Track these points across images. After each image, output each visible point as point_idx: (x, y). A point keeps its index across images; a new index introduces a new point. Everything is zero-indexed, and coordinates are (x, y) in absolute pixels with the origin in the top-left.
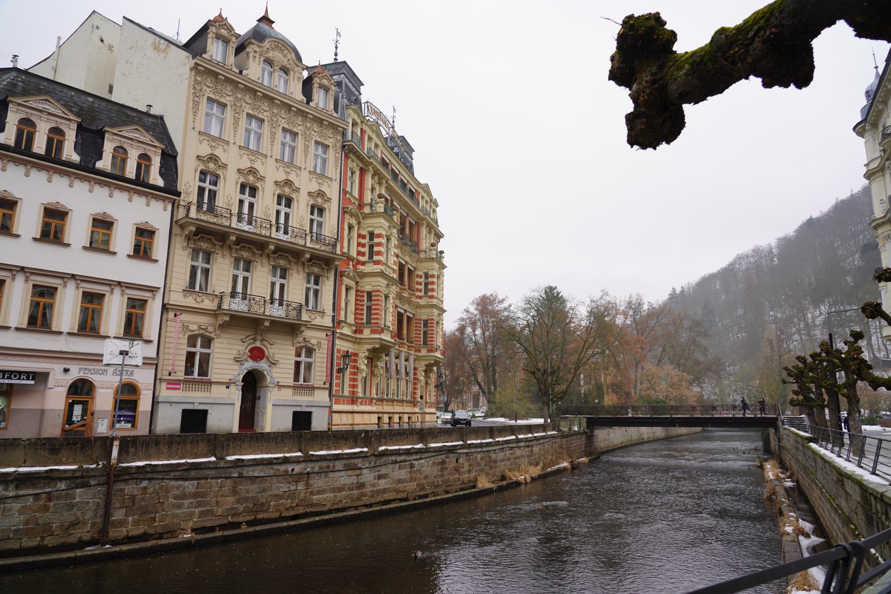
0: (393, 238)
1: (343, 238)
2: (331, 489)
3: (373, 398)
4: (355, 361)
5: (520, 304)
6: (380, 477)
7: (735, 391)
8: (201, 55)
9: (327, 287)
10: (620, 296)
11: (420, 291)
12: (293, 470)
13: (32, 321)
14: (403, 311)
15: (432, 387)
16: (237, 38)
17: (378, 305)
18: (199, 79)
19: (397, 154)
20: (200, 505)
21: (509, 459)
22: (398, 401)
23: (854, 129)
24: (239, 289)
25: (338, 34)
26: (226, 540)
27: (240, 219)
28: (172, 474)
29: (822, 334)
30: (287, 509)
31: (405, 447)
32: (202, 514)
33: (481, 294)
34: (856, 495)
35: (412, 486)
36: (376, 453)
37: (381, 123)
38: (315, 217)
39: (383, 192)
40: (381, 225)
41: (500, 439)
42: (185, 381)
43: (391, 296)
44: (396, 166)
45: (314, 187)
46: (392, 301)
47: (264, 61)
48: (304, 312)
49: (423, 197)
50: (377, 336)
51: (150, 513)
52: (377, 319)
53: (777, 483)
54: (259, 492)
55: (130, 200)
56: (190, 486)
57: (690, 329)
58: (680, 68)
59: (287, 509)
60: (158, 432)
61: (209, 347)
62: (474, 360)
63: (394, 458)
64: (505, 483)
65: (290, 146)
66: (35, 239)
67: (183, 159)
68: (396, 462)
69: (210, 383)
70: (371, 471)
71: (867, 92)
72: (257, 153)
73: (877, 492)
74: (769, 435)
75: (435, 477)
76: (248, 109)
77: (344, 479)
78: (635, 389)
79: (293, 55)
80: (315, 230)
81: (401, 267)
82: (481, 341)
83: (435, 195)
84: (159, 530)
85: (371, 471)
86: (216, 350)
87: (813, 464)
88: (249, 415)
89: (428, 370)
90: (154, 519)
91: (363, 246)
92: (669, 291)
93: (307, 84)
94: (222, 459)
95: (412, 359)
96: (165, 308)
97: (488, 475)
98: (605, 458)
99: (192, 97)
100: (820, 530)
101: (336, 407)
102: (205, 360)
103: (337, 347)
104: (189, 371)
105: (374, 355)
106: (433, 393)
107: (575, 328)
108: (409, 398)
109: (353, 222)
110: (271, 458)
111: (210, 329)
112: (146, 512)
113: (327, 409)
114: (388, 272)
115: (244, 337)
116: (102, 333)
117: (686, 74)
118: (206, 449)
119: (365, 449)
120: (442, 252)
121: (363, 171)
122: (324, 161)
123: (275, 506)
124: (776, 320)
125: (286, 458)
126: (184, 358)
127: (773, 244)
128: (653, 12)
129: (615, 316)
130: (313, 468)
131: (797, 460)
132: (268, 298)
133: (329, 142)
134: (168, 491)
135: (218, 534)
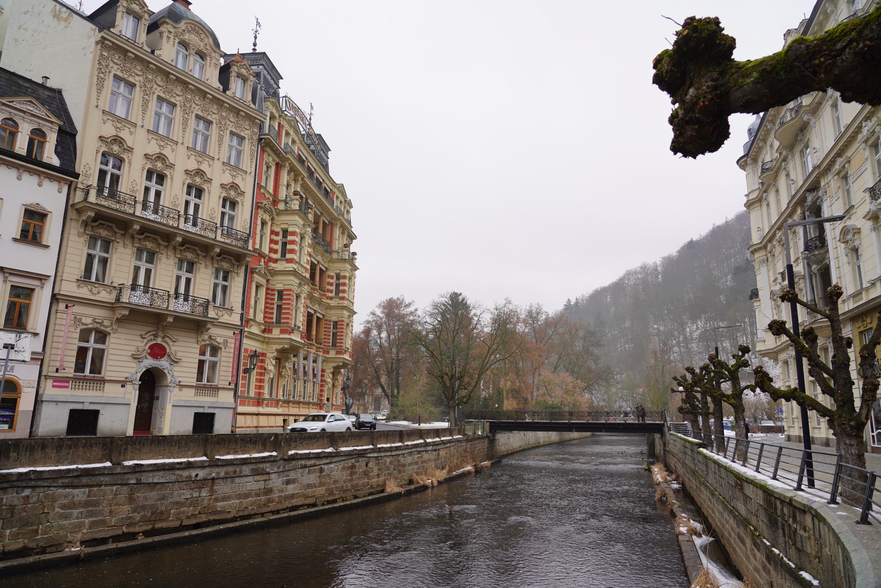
0: (307, 237)
1: (255, 233)
2: (237, 495)
3: (280, 400)
4: (263, 361)
5: (428, 309)
6: (288, 482)
7: (621, 398)
8: (109, 29)
9: (237, 284)
10: (522, 304)
11: (331, 291)
12: (197, 475)
14: (313, 312)
15: (338, 390)
16: (150, 15)
17: (289, 304)
18: (106, 54)
19: (313, 152)
20: (91, 514)
21: (417, 463)
22: (304, 403)
23: (737, 162)
24: (141, 281)
25: (258, 24)
26: (120, 552)
27: (145, 207)
28: (60, 482)
29: (698, 347)
30: (188, 517)
31: (315, 451)
32: (93, 524)
33: (388, 298)
34: (758, 498)
35: (321, 491)
36: (286, 457)
37: (299, 119)
38: (227, 210)
39: (299, 190)
40: (295, 223)
41: (409, 443)
42: (75, 379)
43: (303, 296)
44: (313, 164)
45: (227, 179)
46: (303, 301)
47: (179, 43)
48: (211, 308)
49: (337, 197)
50: (287, 336)
51: (32, 524)
52: (288, 318)
53: (666, 485)
54: (159, 500)
56: (80, 494)
57: (584, 339)
58: (748, 76)
59: (188, 517)
60: (40, 434)
61: (104, 343)
62: (378, 363)
63: (303, 462)
64: (412, 487)
65: (203, 134)
67: (83, 139)
68: (305, 466)
69: (103, 381)
70: (279, 476)
71: (749, 130)
72: (166, 139)
73: (785, 497)
74: (654, 439)
75: (345, 482)
76: (159, 92)
77: (251, 484)
78: (532, 394)
79: (211, 40)
80: (226, 223)
81: (313, 266)
82: (386, 345)
83: (350, 196)
84: (41, 544)
85: (279, 476)
86: (112, 346)
87: (703, 468)
88: (145, 415)
89: (336, 372)
90: (36, 532)
91: (276, 243)
92: (564, 302)
93: (224, 73)
94: (118, 464)
95: (320, 360)
96: (55, 298)
97: (396, 478)
98: (505, 461)
99: (96, 72)
100: (709, 529)
101: (241, 409)
102: (99, 356)
103: (244, 347)
104: (80, 366)
105: (282, 357)
106: (340, 396)
107: (478, 334)
108: (315, 401)
109: (267, 217)
110: (174, 463)
111: (106, 323)
112: (27, 524)
113: (232, 411)
114: (301, 271)
115: (143, 333)
117: (753, 82)
118: (100, 454)
119: (274, 454)
120: (354, 254)
121: (278, 167)
122: (239, 153)
123: (175, 514)
124: (659, 333)
125: (189, 463)
126: (75, 353)
127: (658, 263)
128: (712, 16)
129: (515, 325)
130: (218, 473)
131: (684, 464)
132: (172, 292)
133: (245, 133)
134: (54, 500)
135: (111, 546)
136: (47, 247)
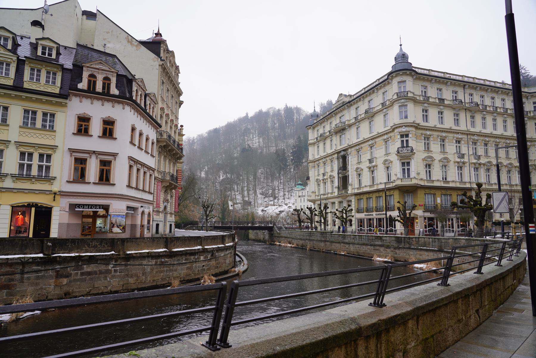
13: (101, 179)
55: (92, 103)
116: (111, 182)
136: (91, 136)
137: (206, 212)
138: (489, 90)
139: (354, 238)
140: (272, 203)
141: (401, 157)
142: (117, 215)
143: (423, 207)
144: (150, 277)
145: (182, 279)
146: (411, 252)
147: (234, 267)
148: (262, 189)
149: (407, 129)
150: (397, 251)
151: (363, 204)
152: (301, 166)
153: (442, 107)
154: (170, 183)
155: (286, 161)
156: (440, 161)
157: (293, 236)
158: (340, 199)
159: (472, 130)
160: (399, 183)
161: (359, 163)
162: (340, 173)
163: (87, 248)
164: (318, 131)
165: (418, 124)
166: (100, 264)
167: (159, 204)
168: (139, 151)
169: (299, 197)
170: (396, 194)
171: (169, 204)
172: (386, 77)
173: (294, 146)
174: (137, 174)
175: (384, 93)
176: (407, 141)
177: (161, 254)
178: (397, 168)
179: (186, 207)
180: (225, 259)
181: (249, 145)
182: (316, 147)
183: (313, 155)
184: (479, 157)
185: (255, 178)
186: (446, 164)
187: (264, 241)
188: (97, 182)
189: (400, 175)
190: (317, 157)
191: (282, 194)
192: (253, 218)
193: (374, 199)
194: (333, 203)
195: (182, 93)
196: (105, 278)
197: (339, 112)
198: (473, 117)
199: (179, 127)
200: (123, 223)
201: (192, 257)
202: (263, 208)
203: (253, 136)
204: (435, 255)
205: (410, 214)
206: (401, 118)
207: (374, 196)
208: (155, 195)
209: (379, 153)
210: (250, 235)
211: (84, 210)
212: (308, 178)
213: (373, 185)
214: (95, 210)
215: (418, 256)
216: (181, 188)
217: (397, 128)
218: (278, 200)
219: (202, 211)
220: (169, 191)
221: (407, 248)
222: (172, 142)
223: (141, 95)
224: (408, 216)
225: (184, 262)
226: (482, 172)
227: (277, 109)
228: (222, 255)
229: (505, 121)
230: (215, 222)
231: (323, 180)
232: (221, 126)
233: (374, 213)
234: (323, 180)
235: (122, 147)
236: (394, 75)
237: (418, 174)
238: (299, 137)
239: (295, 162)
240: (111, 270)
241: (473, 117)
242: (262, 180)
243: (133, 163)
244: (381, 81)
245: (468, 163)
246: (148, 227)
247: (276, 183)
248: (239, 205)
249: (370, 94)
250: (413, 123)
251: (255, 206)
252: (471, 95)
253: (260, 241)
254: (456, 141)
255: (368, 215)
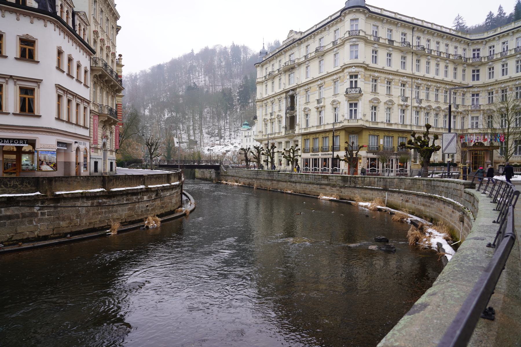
66: (16, 59)
116: (36, 114)
136: (6, 57)
137: (150, 150)
138: (436, 35)
139: (300, 178)
140: (218, 142)
141: (350, 98)
142: (45, 151)
143: (367, 148)
144: (86, 220)
145: (124, 221)
146: (356, 191)
147: (181, 206)
148: (208, 128)
149: (357, 69)
150: (343, 190)
151: (310, 144)
152: (247, 106)
153: (391, 49)
154: (109, 118)
155: (233, 100)
156: (385, 103)
157: (240, 175)
158: (287, 139)
159: (417, 74)
160: (346, 124)
161: (307, 103)
162: (288, 113)
163: (5, 188)
164: (266, 69)
165: (368, 65)
166: (22, 206)
167: (97, 140)
168: (69, 79)
169: (245, 137)
170: (342, 134)
171: (109, 141)
172: (339, 14)
173: (240, 85)
174: (77, 109)
175: (335, 31)
176: (356, 82)
177: (98, 194)
178: (344, 109)
179: (129, 145)
180: (171, 199)
181: (194, 83)
182: (264, 85)
183: (261, 94)
184: (420, 101)
185: (201, 117)
186: (391, 106)
187: (211, 180)
188: (18, 112)
189: (347, 116)
190: (265, 96)
191: (228, 133)
192: (199, 157)
193: (321, 139)
194: (280, 143)
195: (119, 17)
196: (31, 222)
197: (289, 50)
198: (418, 61)
199: (117, 57)
200: (54, 160)
201: (135, 197)
202: (209, 147)
203: (199, 74)
204: (379, 193)
205: (356, 154)
206: (351, 58)
207: (320, 136)
208: (92, 131)
209: (328, 94)
210: (196, 173)
211: (4, 144)
212: (255, 118)
213: (320, 126)
214: (19, 145)
215: (363, 195)
216: (122, 124)
217: (347, 68)
218: (224, 139)
219: (146, 149)
220: (108, 127)
221: (353, 187)
222: (109, 71)
223: (67, 12)
224: (354, 156)
225: (125, 202)
226: (422, 115)
227: (224, 46)
228: (168, 194)
229: (447, 67)
230: (160, 161)
231: (271, 120)
232: (165, 62)
233: (320, 153)
234: (271, 120)
235: (46, 72)
236: (347, 11)
237: (365, 115)
238: (246, 77)
239: (241, 102)
240: (37, 214)
241: (418, 61)
242: (208, 119)
243: (62, 92)
244: (333, 17)
245: (410, 107)
246: (84, 165)
247: (222, 123)
248: (185, 144)
249: (321, 32)
250: (363, 63)
251: (201, 145)
252: (419, 38)
253: (206, 180)
254: (401, 84)
255: (314, 155)
